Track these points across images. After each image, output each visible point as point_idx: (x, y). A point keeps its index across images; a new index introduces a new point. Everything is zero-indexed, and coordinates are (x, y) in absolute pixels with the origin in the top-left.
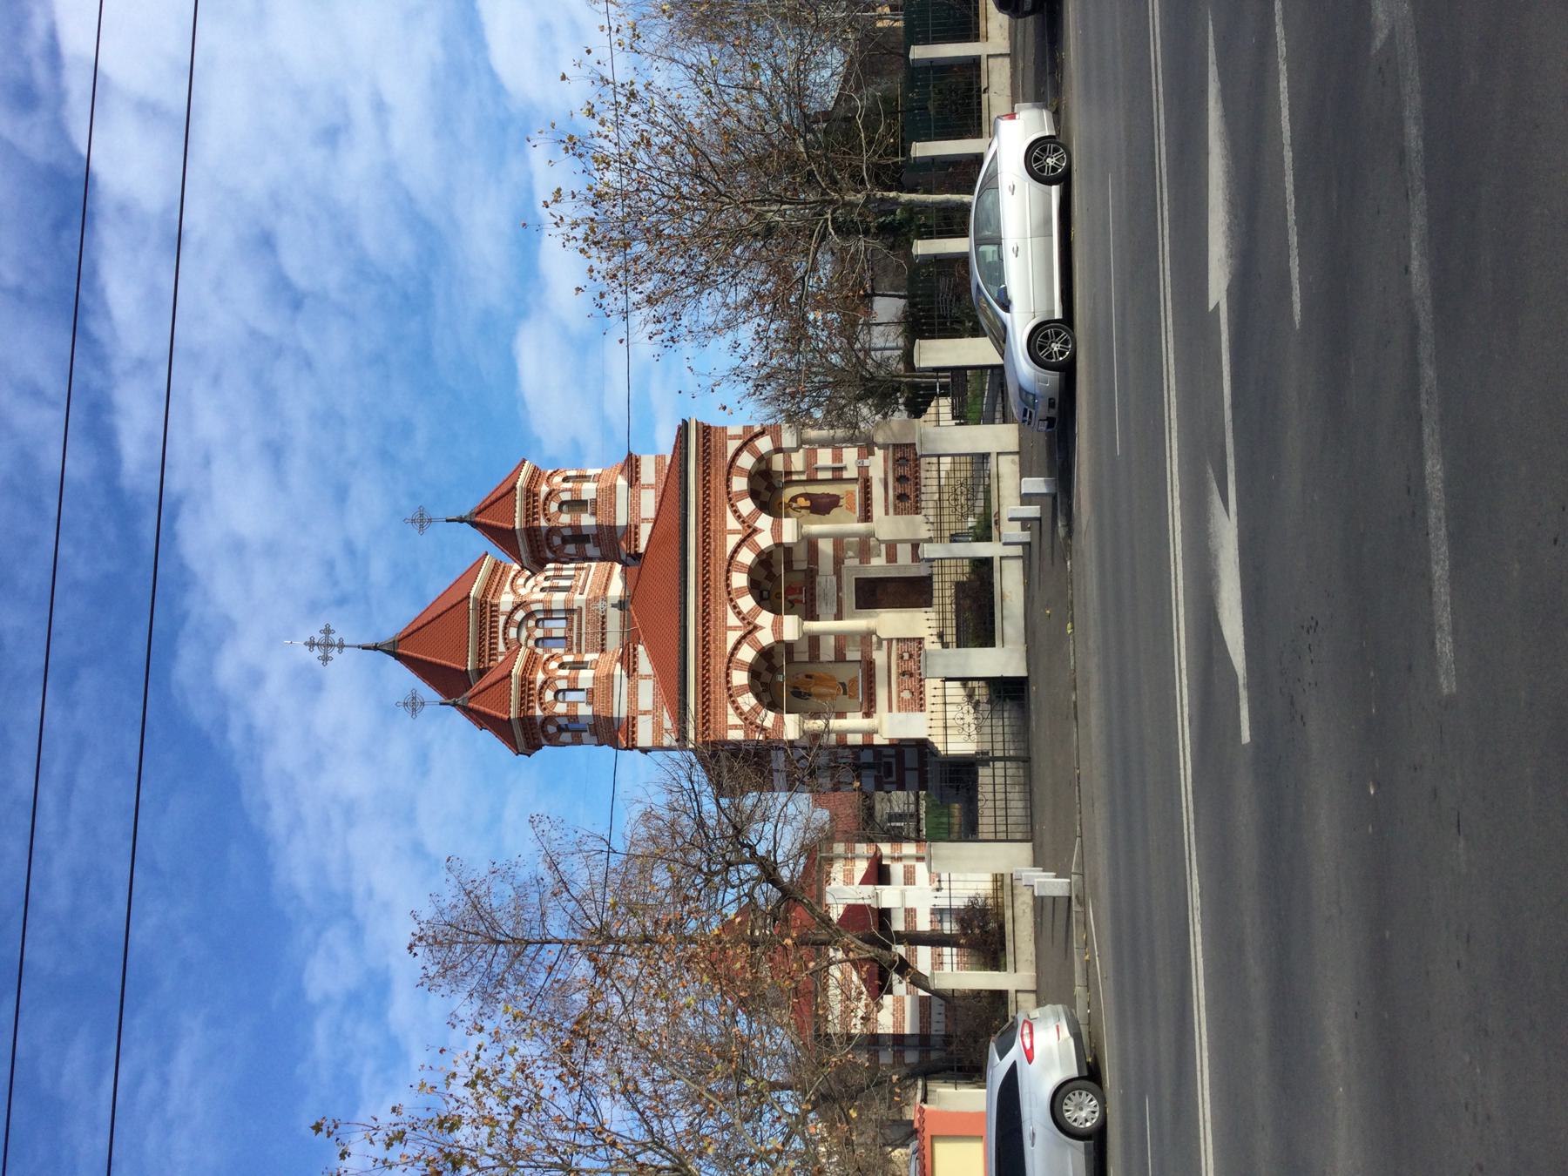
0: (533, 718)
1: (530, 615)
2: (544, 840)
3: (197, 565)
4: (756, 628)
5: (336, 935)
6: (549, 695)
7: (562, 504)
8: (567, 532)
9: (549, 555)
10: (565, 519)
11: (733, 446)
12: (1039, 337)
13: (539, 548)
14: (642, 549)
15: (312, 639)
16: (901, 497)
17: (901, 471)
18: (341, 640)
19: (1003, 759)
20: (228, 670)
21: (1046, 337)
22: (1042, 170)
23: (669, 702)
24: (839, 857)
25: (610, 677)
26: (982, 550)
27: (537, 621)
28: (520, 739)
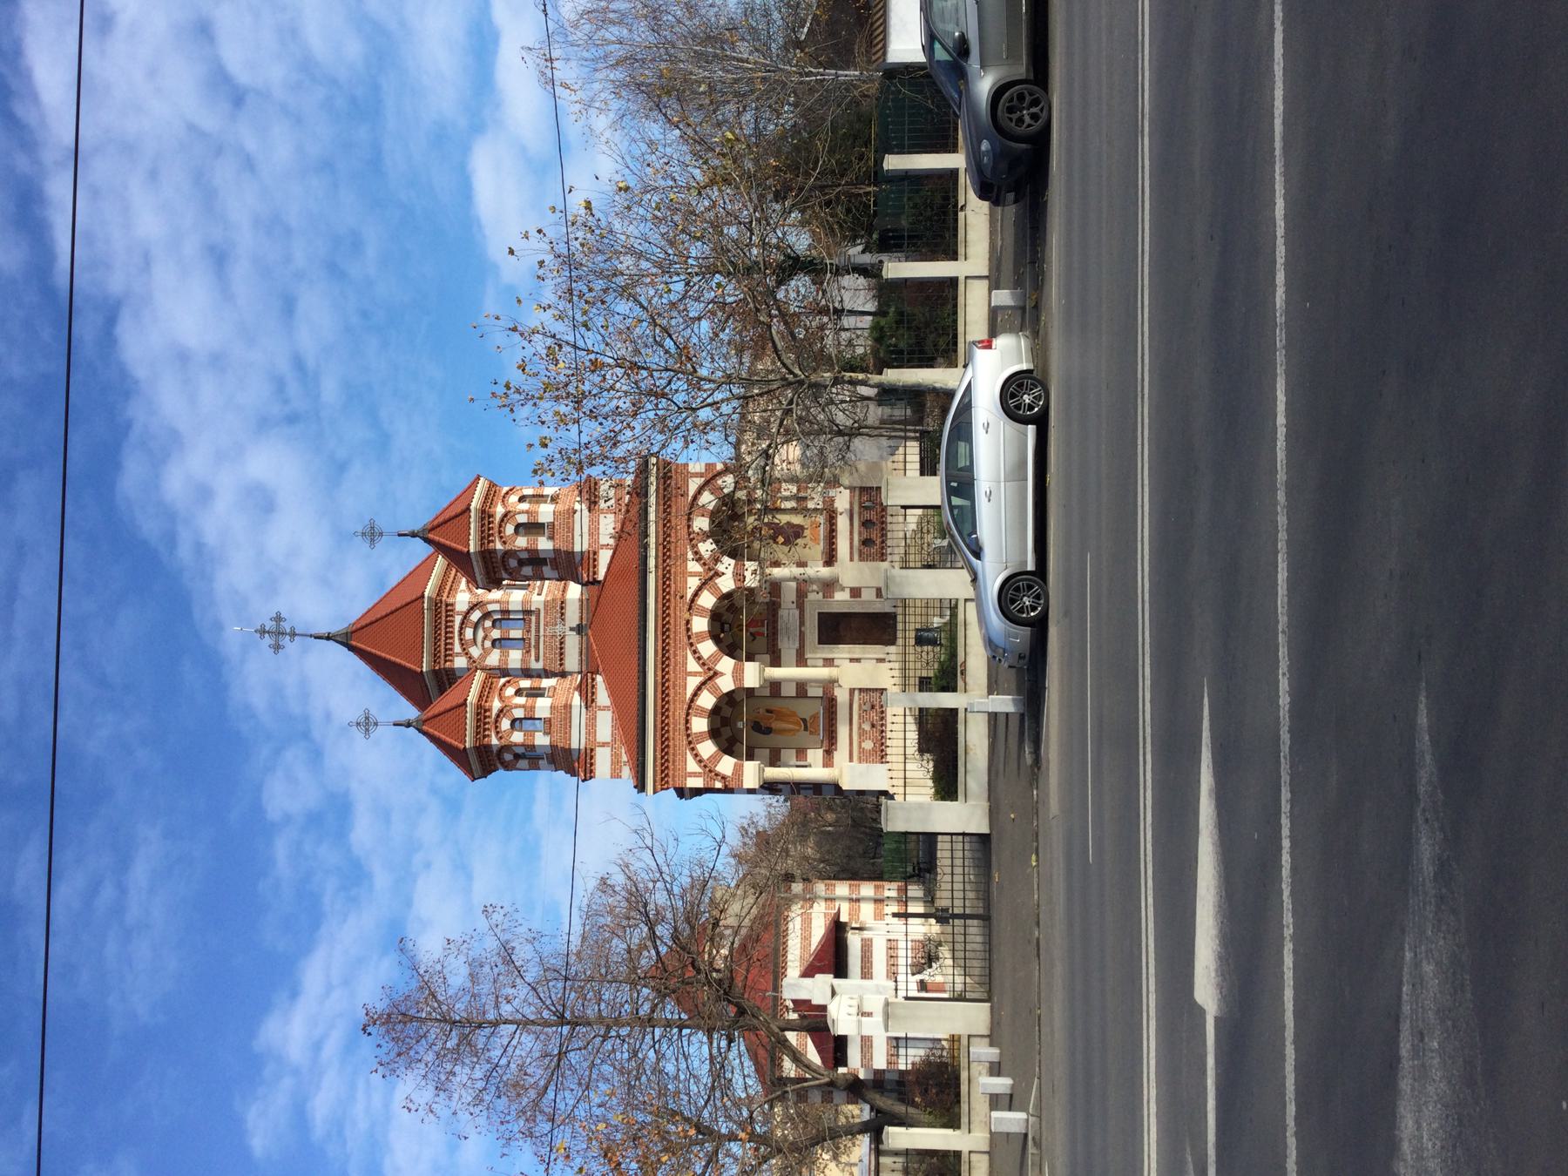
0: (489, 746)
1: (487, 615)
2: (498, 931)
3: (141, 373)
4: (716, 674)
5: (294, 756)
6: (505, 724)
7: (518, 527)
8: (524, 556)
9: (505, 575)
10: (522, 542)
11: (693, 485)
12: (1011, 590)
13: (495, 569)
14: (601, 577)
15: (263, 626)
16: (866, 542)
17: (867, 516)
18: (293, 629)
19: (964, 916)
20: (175, 484)
21: (1017, 589)
22: (1018, 407)
23: (627, 743)
24: (796, 896)
25: (568, 707)
26: (945, 700)
27: (494, 622)
28: (475, 765)
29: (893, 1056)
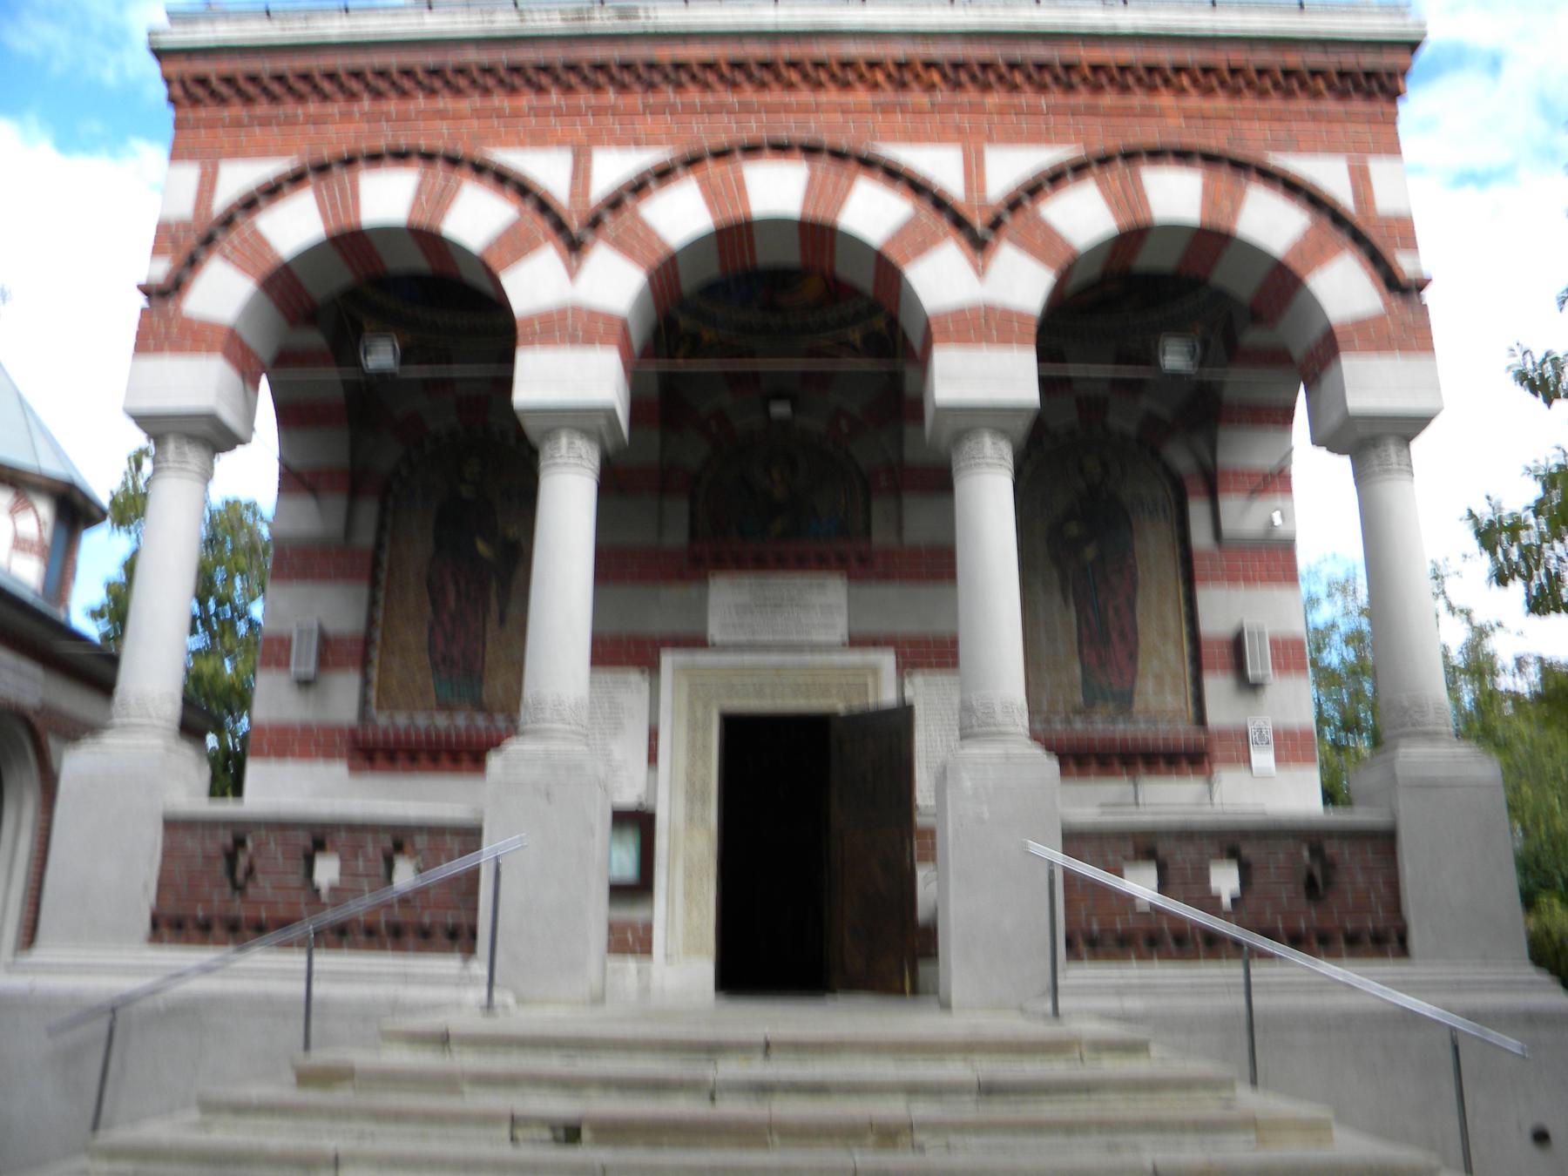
11: (1329, 174)
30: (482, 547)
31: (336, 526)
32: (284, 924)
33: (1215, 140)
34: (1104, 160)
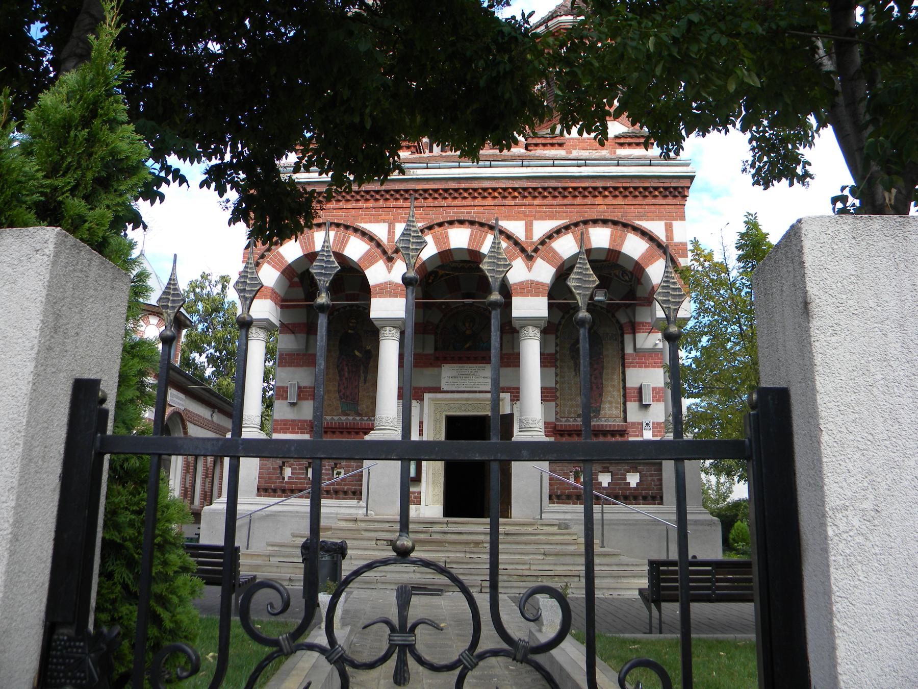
4: (390, 260)
11: (657, 228)
29: (414, 493)
30: (357, 353)
31: (303, 347)
32: (301, 491)
33: (617, 215)
34: (576, 225)
